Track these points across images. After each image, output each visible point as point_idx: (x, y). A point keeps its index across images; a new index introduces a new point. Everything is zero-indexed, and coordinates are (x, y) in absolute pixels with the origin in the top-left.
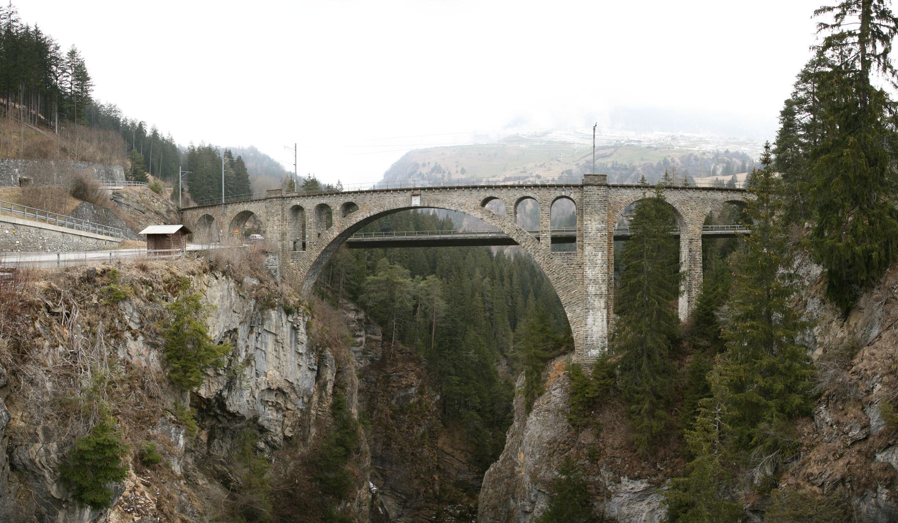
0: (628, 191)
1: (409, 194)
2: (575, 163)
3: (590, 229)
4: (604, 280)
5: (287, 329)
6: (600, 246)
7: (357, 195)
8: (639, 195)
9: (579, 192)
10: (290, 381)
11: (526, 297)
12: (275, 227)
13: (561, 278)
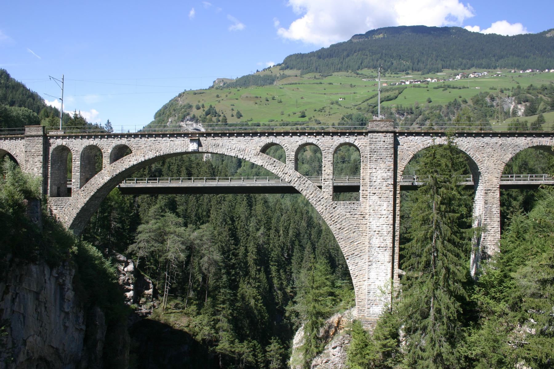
2: (356, 107)
5: (51, 286)
6: (385, 196)
10: (55, 346)
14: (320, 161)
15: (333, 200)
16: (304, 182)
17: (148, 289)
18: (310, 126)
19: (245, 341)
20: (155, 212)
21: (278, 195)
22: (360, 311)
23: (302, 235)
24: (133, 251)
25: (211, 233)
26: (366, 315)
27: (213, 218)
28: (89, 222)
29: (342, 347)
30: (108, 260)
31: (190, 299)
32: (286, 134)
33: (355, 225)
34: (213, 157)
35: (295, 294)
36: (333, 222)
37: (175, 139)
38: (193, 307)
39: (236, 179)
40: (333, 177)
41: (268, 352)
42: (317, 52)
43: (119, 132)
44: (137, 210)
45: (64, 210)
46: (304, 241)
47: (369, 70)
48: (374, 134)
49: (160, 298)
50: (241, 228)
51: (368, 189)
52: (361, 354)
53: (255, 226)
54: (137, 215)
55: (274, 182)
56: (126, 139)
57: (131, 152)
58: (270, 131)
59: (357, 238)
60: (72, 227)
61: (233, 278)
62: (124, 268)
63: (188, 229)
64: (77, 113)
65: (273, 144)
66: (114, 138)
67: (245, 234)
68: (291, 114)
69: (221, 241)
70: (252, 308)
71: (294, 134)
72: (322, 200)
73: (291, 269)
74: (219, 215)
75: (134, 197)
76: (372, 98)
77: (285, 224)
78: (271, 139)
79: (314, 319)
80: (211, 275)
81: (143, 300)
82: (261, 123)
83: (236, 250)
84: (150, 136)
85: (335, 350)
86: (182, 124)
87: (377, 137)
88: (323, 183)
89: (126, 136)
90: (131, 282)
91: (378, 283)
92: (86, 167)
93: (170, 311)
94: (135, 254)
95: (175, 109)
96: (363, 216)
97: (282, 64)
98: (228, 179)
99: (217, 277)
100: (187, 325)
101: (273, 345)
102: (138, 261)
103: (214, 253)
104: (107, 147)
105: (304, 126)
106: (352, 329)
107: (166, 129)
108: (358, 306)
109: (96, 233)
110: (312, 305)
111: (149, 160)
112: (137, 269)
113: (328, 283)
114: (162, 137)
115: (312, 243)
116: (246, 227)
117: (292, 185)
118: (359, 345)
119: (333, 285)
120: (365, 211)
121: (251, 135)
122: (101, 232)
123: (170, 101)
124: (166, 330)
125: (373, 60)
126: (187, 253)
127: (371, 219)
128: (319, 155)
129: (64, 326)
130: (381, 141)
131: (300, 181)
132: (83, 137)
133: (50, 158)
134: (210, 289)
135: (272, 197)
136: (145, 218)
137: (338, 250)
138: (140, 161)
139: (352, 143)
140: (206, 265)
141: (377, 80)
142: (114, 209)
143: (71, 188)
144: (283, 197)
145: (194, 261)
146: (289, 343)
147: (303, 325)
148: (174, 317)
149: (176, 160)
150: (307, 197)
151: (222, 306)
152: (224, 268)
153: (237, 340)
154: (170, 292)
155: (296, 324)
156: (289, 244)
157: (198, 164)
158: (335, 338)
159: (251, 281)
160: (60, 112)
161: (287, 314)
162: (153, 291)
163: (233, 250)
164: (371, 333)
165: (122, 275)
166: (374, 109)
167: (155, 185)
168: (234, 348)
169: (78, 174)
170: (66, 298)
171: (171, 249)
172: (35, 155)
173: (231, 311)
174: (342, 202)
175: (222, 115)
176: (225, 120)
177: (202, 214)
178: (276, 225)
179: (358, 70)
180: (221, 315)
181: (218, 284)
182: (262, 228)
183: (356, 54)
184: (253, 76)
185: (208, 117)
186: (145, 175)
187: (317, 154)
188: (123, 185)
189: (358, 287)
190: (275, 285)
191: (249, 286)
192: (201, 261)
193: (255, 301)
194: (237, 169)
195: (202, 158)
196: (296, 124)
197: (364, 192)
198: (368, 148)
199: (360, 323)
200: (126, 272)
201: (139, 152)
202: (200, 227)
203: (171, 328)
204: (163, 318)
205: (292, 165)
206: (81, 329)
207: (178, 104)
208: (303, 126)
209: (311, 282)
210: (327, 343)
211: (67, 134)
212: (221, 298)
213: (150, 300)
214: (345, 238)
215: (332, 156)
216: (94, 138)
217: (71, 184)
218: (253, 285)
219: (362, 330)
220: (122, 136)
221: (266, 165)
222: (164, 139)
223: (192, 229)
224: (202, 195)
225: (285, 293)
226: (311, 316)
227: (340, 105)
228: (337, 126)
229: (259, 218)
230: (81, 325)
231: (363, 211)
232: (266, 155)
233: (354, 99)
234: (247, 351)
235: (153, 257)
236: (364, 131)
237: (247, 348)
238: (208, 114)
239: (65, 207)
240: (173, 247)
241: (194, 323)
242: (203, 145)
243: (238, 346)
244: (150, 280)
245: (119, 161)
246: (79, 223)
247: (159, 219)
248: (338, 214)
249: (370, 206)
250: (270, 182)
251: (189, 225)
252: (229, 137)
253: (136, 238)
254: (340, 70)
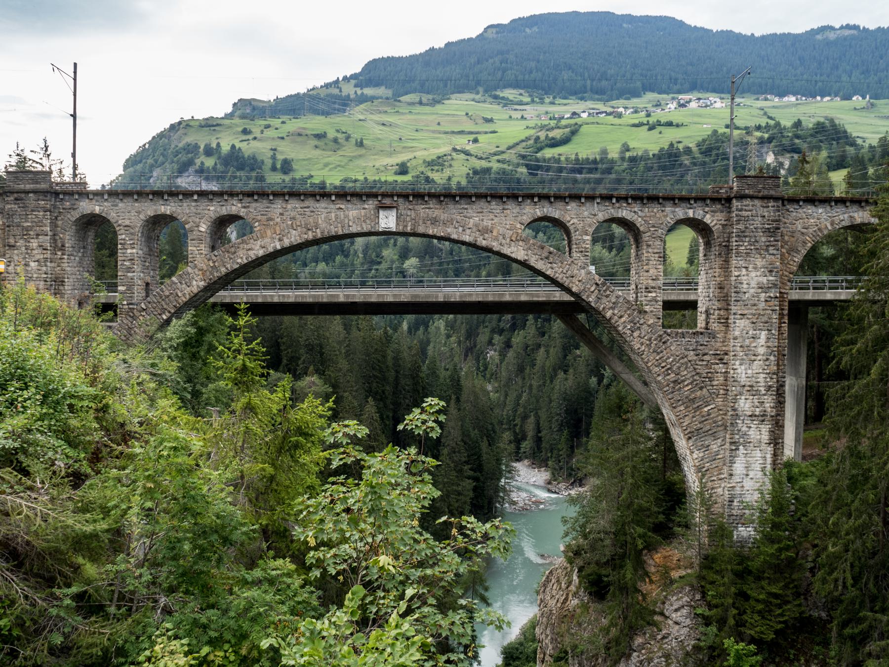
0: (820, 211)
1: (371, 204)
3: (745, 286)
4: (770, 387)
6: (765, 319)
7: (250, 199)
8: (841, 217)
9: (722, 212)
11: (613, 107)
12: (32, 264)
13: (683, 381)
96: (719, 357)
104: (198, 220)
172: (31, 233)
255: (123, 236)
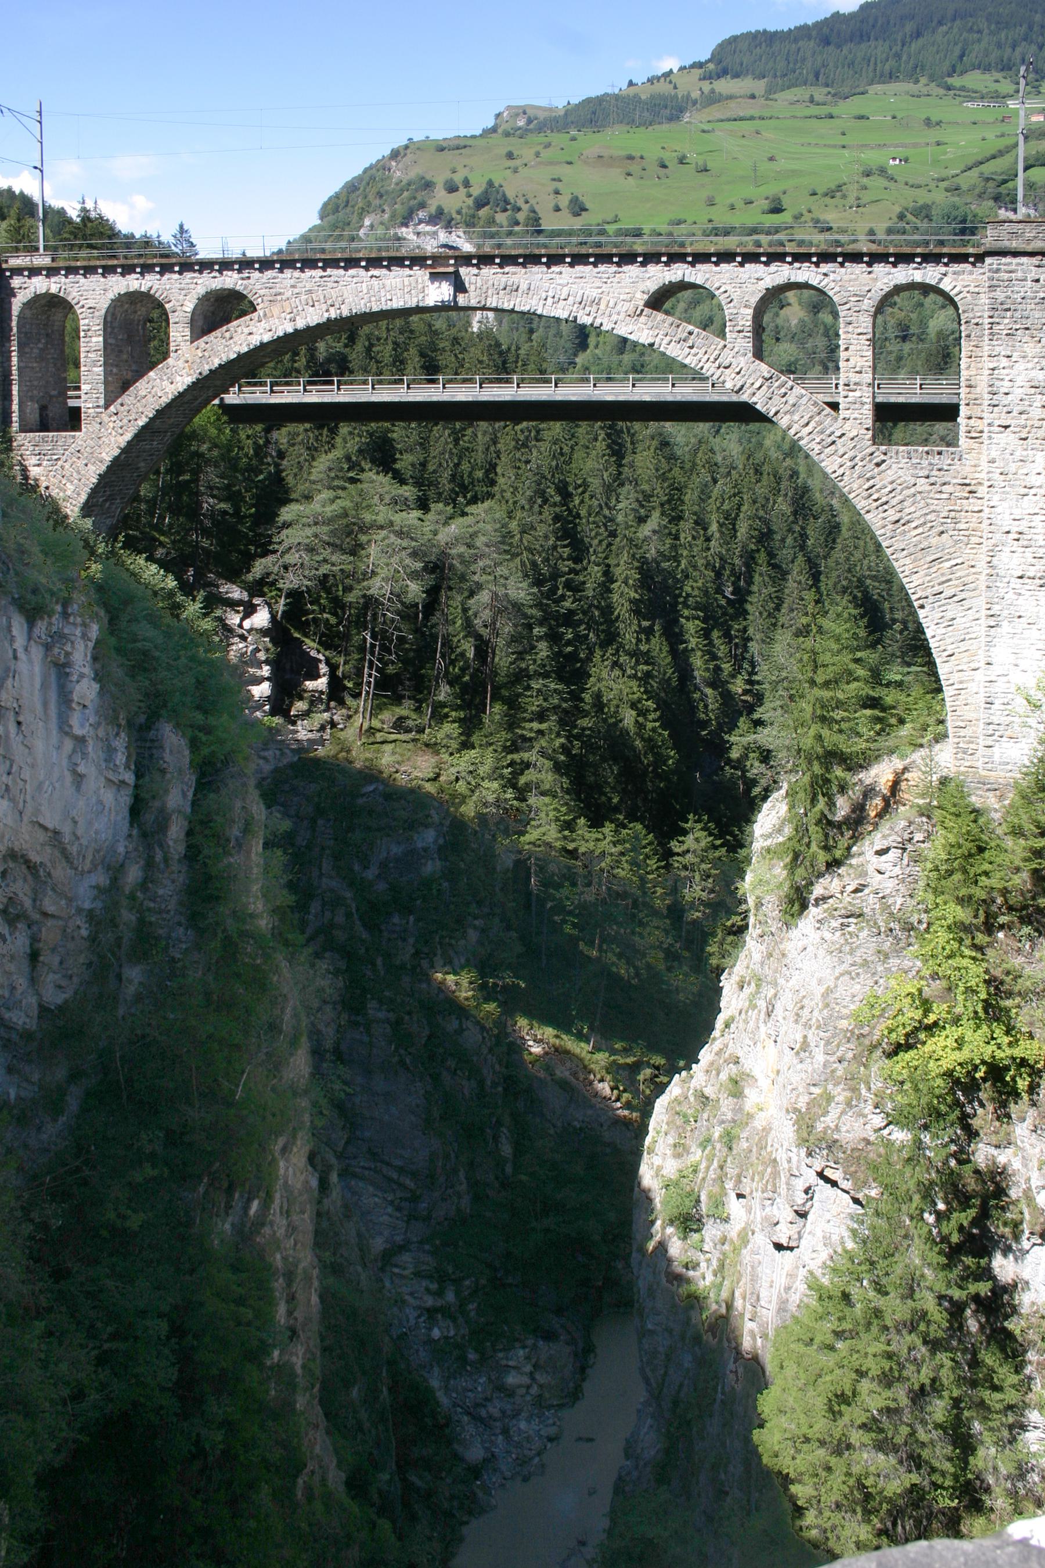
10: (50, 826)
14: (832, 335)
15: (874, 441)
16: (783, 390)
17: (316, 676)
18: (798, 237)
19: (607, 824)
20: (330, 469)
21: (701, 424)
22: (962, 752)
23: (778, 537)
24: (268, 574)
25: (498, 526)
26: (979, 764)
27: (505, 487)
28: (136, 498)
29: (904, 849)
30: (194, 600)
31: (438, 706)
32: (725, 257)
33: (945, 514)
34: (500, 323)
35: (760, 698)
36: (876, 504)
37: (384, 271)
38: (450, 729)
39: (572, 381)
40: (874, 379)
41: (678, 854)
42: (817, 25)
43: (216, 255)
44: (277, 465)
45: (62, 467)
46: (785, 554)
47: (987, 76)
48: (1004, 260)
49: (349, 701)
50: (590, 515)
51: (985, 415)
52: (965, 872)
53: (633, 509)
54: (278, 479)
55: (690, 390)
56: (235, 275)
57: (255, 310)
58: (676, 249)
59: (952, 550)
60: (87, 509)
61: (569, 649)
62: (242, 620)
63: (431, 516)
64: (89, 205)
65: (683, 286)
66: (201, 272)
67: (602, 530)
68: (739, 205)
69: (530, 550)
70: (628, 734)
71: (751, 258)
72: (839, 442)
73: (745, 630)
74: (523, 478)
75: (268, 430)
76: (994, 157)
77: (726, 507)
78: (678, 272)
79: (817, 769)
80: (501, 642)
81: (300, 706)
82: (646, 230)
83: (577, 573)
84: (309, 264)
85: (884, 858)
86: (403, 231)
87: (1013, 267)
88: (843, 393)
89: (236, 267)
90: (263, 658)
91: (1017, 678)
92: (121, 351)
93: (379, 736)
94: (273, 584)
95: (382, 191)
96: (968, 488)
97: (707, 62)
98: (548, 381)
99: (520, 648)
100: (432, 775)
101: (691, 836)
102: (282, 601)
103: (511, 582)
105: (781, 236)
106: (935, 803)
107: (354, 245)
108: (956, 740)
109: (157, 528)
110: (812, 732)
111: (308, 329)
112: (280, 623)
113: (861, 672)
114: (346, 268)
115: (809, 560)
116: (606, 512)
117: (744, 397)
118: (960, 846)
119: (876, 677)
120: (977, 475)
121: (615, 259)
122: (171, 526)
123: (366, 171)
124: (371, 788)
125: (999, 46)
126: (430, 580)
127: (996, 497)
128: (828, 319)
129: (74, 772)
130: (1025, 280)
131: (769, 387)
132: (108, 270)
133: (15, 330)
134: (501, 679)
135: (683, 432)
136: (302, 488)
137: (889, 582)
138: (281, 334)
139: (933, 282)
140: (486, 615)
141: (1012, 104)
142: (207, 463)
143: (79, 408)
144: (718, 432)
145: (451, 602)
146: (742, 832)
147: (785, 786)
148: (394, 753)
149: (388, 330)
150: (792, 432)
151: (535, 725)
152: (541, 624)
153: (582, 821)
154: (378, 685)
155: (763, 782)
156: (737, 561)
157: (456, 341)
158: (885, 827)
159: (623, 659)
160: (37, 205)
161: (735, 754)
162: (330, 684)
163: (569, 573)
164: (997, 816)
165: (236, 640)
166: (1003, 190)
167: (327, 398)
168: (573, 841)
169: (100, 370)
170: (76, 699)
171: (379, 570)
173: (562, 740)
174: (902, 448)
175: (525, 207)
176: (535, 219)
177: (470, 474)
178: (696, 508)
179: (950, 75)
180: (534, 751)
181: (523, 666)
182: (656, 514)
183: (945, 28)
184: (616, 97)
185: (483, 212)
186: (298, 371)
187: (820, 315)
188: (232, 398)
189: (956, 686)
190: (696, 673)
191: (617, 672)
192: (472, 601)
193: (638, 715)
194: (576, 355)
195: (469, 324)
196: (754, 231)
197: (972, 422)
198: (984, 299)
199: (960, 786)
200: (249, 631)
201: (276, 310)
202: (468, 509)
203: (385, 782)
204: (360, 755)
205: (745, 344)
206: (123, 782)
207: (390, 178)
208: (776, 237)
209: (809, 668)
210: (855, 838)
211: (61, 264)
212: (534, 704)
213: (322, 707)
214: (912, 550)
215: (870, 320)
216: (142, 274)
217: (79, 397)
218: (629, 672)
219: (967, 806)
220: (225, 265)
221: (665, 341)
222: (352, 272)
223: (442, 518)
224: (471, 425)
225: (727, 697)
226: (810, 763)
227: (892, 179)
228: (881, 236)
229: (645, 487)
230: (121, 770)
231: (970, 476)
232: (664, 316)
233: (936, 162)
234: (613, 850)
235: (328, 591)
236: (971, 250)
237: (615, 844)
238: (483, 206)
239: (64, 458)
240: (387, 565)
241: (453, 770)
242: (471, 288)
243: (587, 835)
244: (319, 652)
245: (218, 333)
246: (106, 501)
247: (344, 488)
248: (892, 483)
249: (993, 461)
250: (675, 390)
251: (432, 505)
252: (548, 265)
253: (275, 539)
254: (891, 77)
255: (86, 321)
